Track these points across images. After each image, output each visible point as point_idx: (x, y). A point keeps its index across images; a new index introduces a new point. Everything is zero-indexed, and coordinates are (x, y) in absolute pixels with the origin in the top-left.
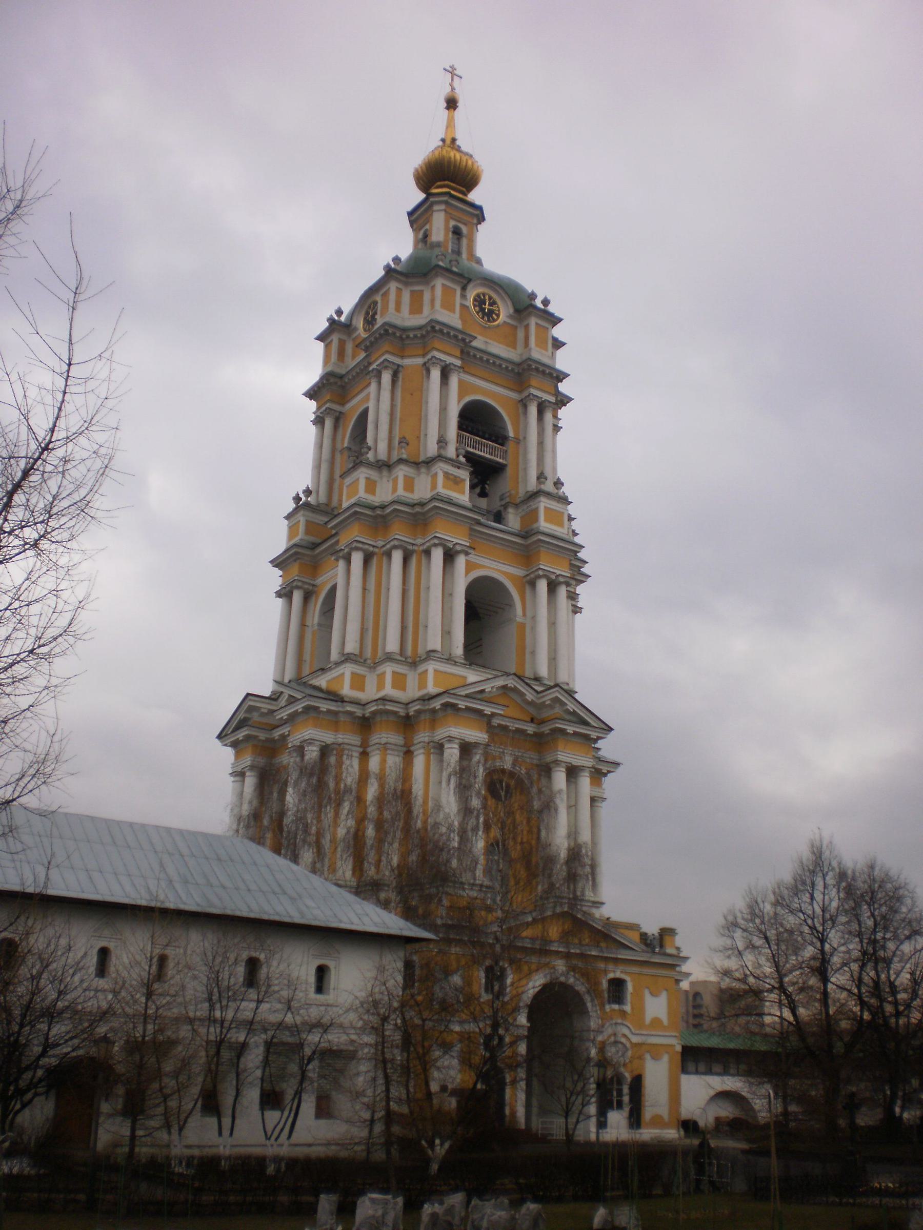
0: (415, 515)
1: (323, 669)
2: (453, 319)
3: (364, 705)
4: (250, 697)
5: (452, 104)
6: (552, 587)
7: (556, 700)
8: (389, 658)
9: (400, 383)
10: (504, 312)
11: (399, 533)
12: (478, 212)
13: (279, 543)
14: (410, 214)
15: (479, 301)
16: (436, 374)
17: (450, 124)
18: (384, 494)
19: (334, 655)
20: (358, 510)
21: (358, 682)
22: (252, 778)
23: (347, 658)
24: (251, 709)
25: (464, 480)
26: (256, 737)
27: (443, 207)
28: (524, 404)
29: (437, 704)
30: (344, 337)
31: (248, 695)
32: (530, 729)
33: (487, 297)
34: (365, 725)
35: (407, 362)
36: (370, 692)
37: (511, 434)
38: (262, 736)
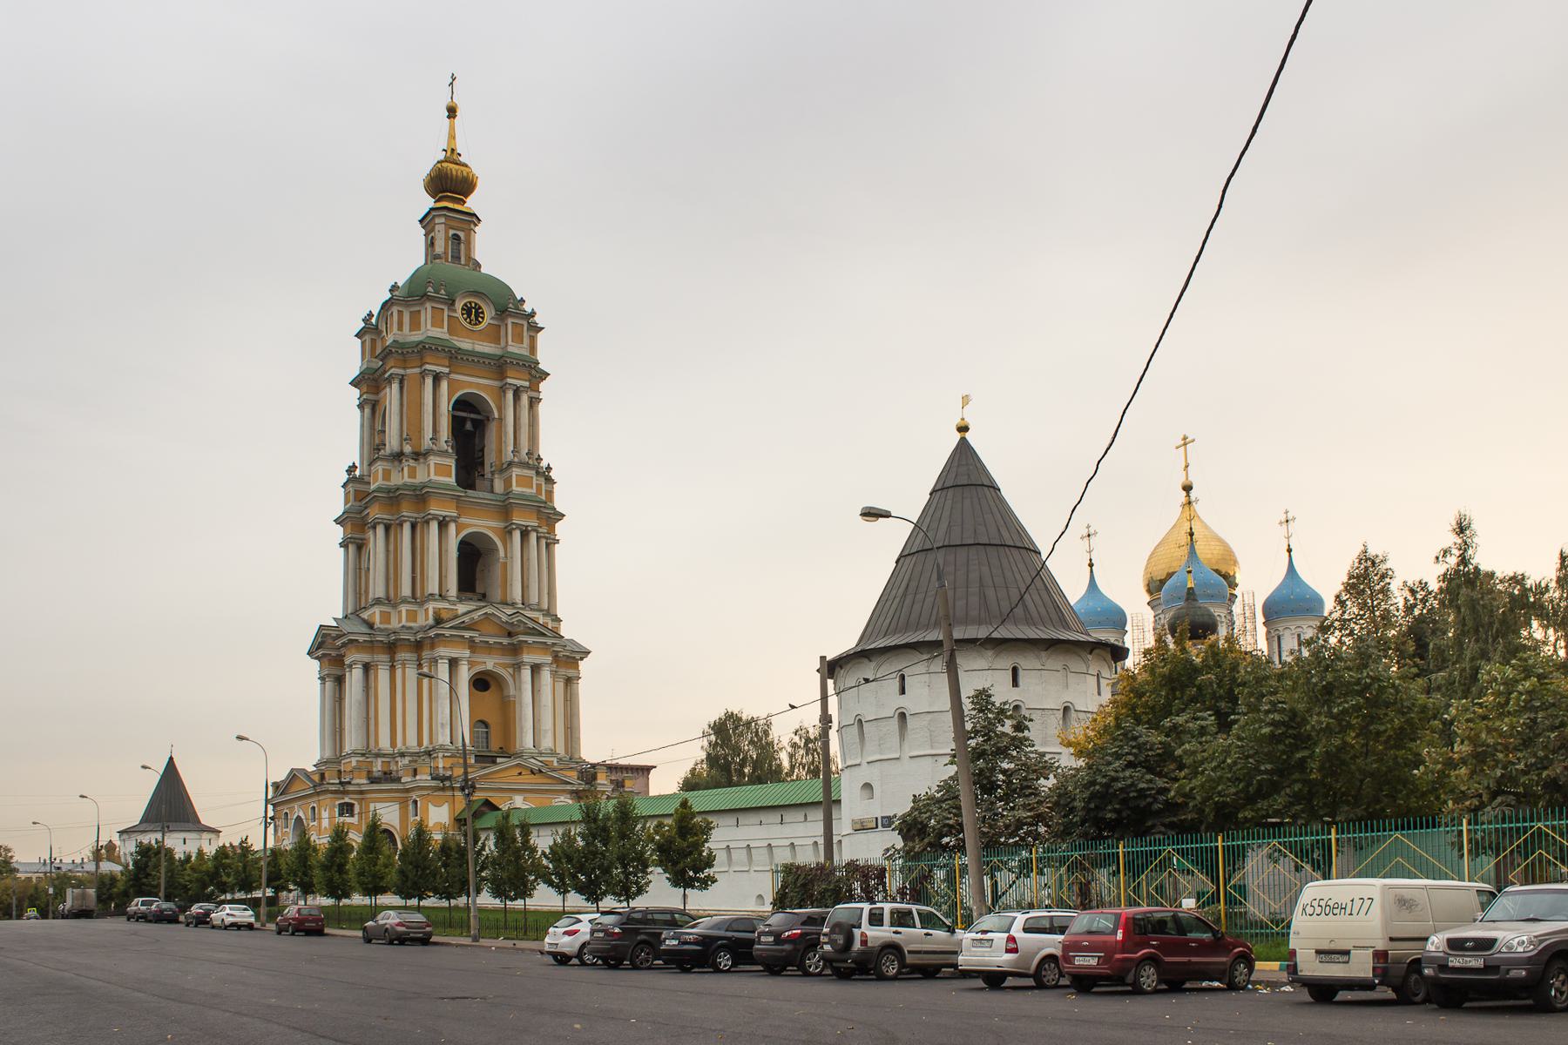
2: (441, 333)
5: (452, 112)
7: (520, 621)
8: (404, 601)
13: (339, 508)
14: (421, 221)
15: (467, 310)
16: (429, 381)
17: (452, 136)
18: (397, 479)
21: (386, 617)
23: (378, 602)
24: (325, 636)
27: (443, 220)
28: (503, 390)
32: (505, 641)
33: (473, 305)
35: (409, 371)
36: (394, 624)
37: (496, 415)
38: (334, 653)
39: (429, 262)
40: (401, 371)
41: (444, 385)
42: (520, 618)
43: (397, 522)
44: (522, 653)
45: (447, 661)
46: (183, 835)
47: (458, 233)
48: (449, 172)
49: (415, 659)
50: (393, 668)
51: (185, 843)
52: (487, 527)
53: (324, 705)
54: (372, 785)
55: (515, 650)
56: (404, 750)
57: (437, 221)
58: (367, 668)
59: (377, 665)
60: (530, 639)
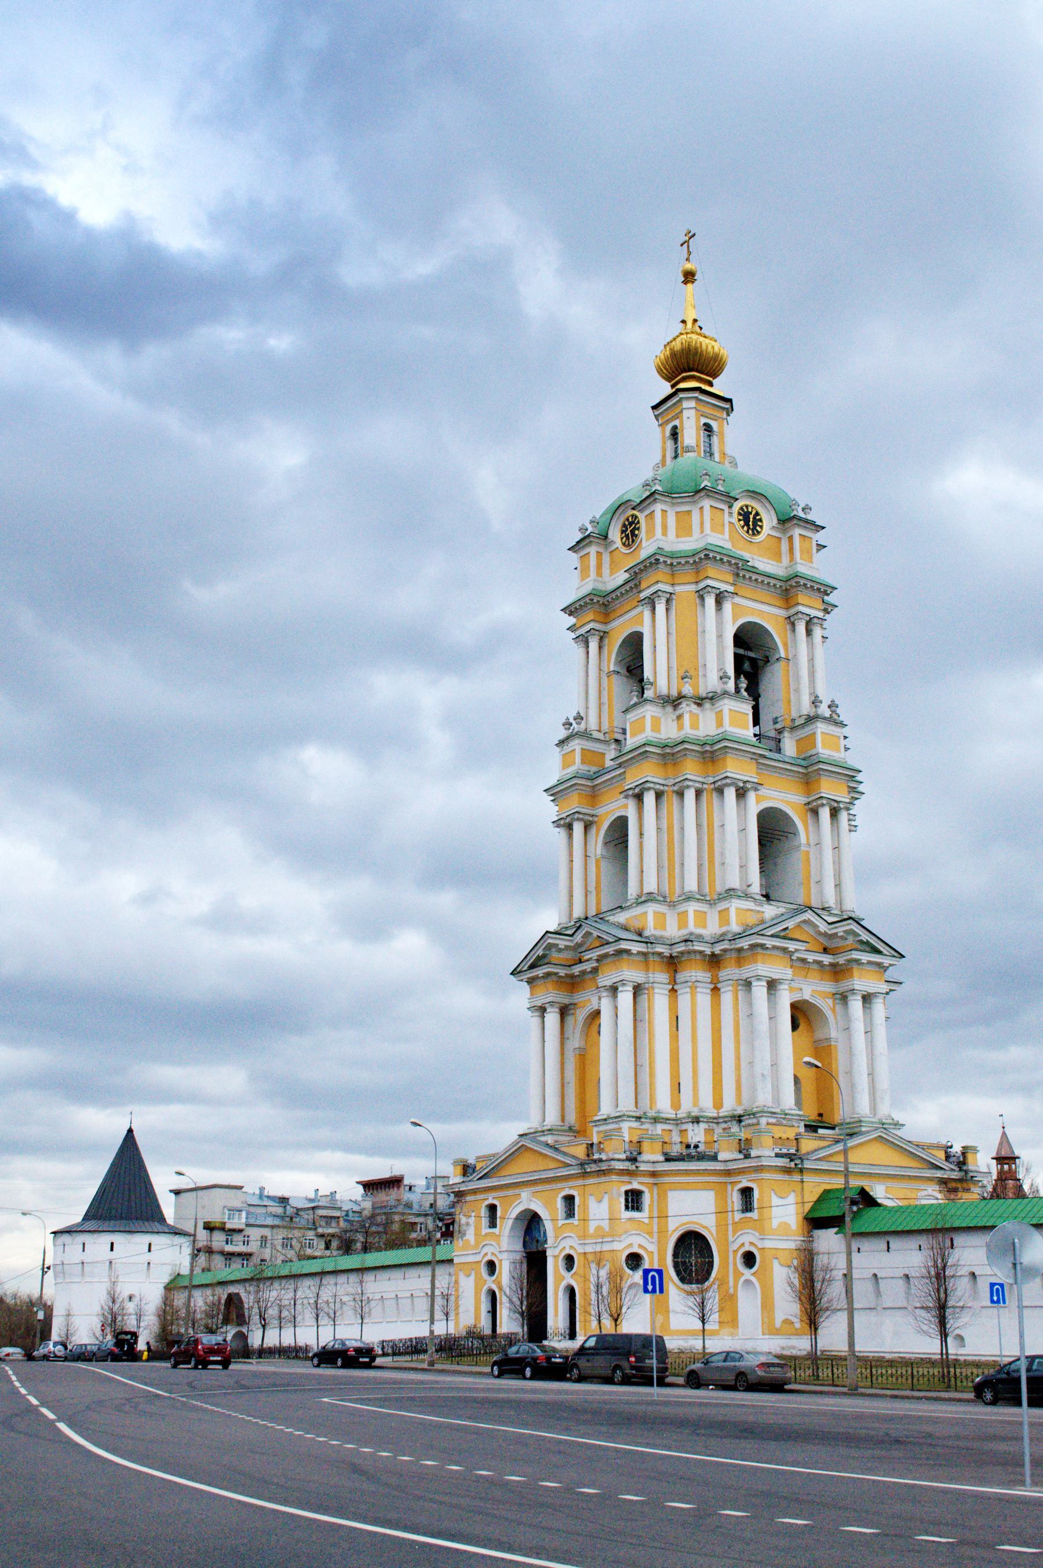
1: (620, 907)
4: (549, 935)
6: (834, 813)
9: (673, 612)
10: (768, 521)
11: (691, 770)
12: (727, 406)
18: (669, 730)
19: (633, 890)
20: (647, 749)
22: (555, 1014)
24: (550, 947)
25: (748, 714)
26: (556, 974)
27: (692, 404)
29: (744, 944)
30: (601, 550)
31: (547, 932)
34: (673, 963)
35: (678, 588)
40: (669, 589)
41: (727, 606)
42: (851, 927)
43: (676, 788)
44: (852, 976)
45: (765, 984)
46: (146, 1239)
48: (698, 345)
49: (709, 980)
50: (716, 990)
51: (112, 1249)
52: (782, 801)
53: (650, 1043)
55: (837, 972)
56: (695, 1112)
58: (638, 990)
59: (653, 988)
60: (865, 957)
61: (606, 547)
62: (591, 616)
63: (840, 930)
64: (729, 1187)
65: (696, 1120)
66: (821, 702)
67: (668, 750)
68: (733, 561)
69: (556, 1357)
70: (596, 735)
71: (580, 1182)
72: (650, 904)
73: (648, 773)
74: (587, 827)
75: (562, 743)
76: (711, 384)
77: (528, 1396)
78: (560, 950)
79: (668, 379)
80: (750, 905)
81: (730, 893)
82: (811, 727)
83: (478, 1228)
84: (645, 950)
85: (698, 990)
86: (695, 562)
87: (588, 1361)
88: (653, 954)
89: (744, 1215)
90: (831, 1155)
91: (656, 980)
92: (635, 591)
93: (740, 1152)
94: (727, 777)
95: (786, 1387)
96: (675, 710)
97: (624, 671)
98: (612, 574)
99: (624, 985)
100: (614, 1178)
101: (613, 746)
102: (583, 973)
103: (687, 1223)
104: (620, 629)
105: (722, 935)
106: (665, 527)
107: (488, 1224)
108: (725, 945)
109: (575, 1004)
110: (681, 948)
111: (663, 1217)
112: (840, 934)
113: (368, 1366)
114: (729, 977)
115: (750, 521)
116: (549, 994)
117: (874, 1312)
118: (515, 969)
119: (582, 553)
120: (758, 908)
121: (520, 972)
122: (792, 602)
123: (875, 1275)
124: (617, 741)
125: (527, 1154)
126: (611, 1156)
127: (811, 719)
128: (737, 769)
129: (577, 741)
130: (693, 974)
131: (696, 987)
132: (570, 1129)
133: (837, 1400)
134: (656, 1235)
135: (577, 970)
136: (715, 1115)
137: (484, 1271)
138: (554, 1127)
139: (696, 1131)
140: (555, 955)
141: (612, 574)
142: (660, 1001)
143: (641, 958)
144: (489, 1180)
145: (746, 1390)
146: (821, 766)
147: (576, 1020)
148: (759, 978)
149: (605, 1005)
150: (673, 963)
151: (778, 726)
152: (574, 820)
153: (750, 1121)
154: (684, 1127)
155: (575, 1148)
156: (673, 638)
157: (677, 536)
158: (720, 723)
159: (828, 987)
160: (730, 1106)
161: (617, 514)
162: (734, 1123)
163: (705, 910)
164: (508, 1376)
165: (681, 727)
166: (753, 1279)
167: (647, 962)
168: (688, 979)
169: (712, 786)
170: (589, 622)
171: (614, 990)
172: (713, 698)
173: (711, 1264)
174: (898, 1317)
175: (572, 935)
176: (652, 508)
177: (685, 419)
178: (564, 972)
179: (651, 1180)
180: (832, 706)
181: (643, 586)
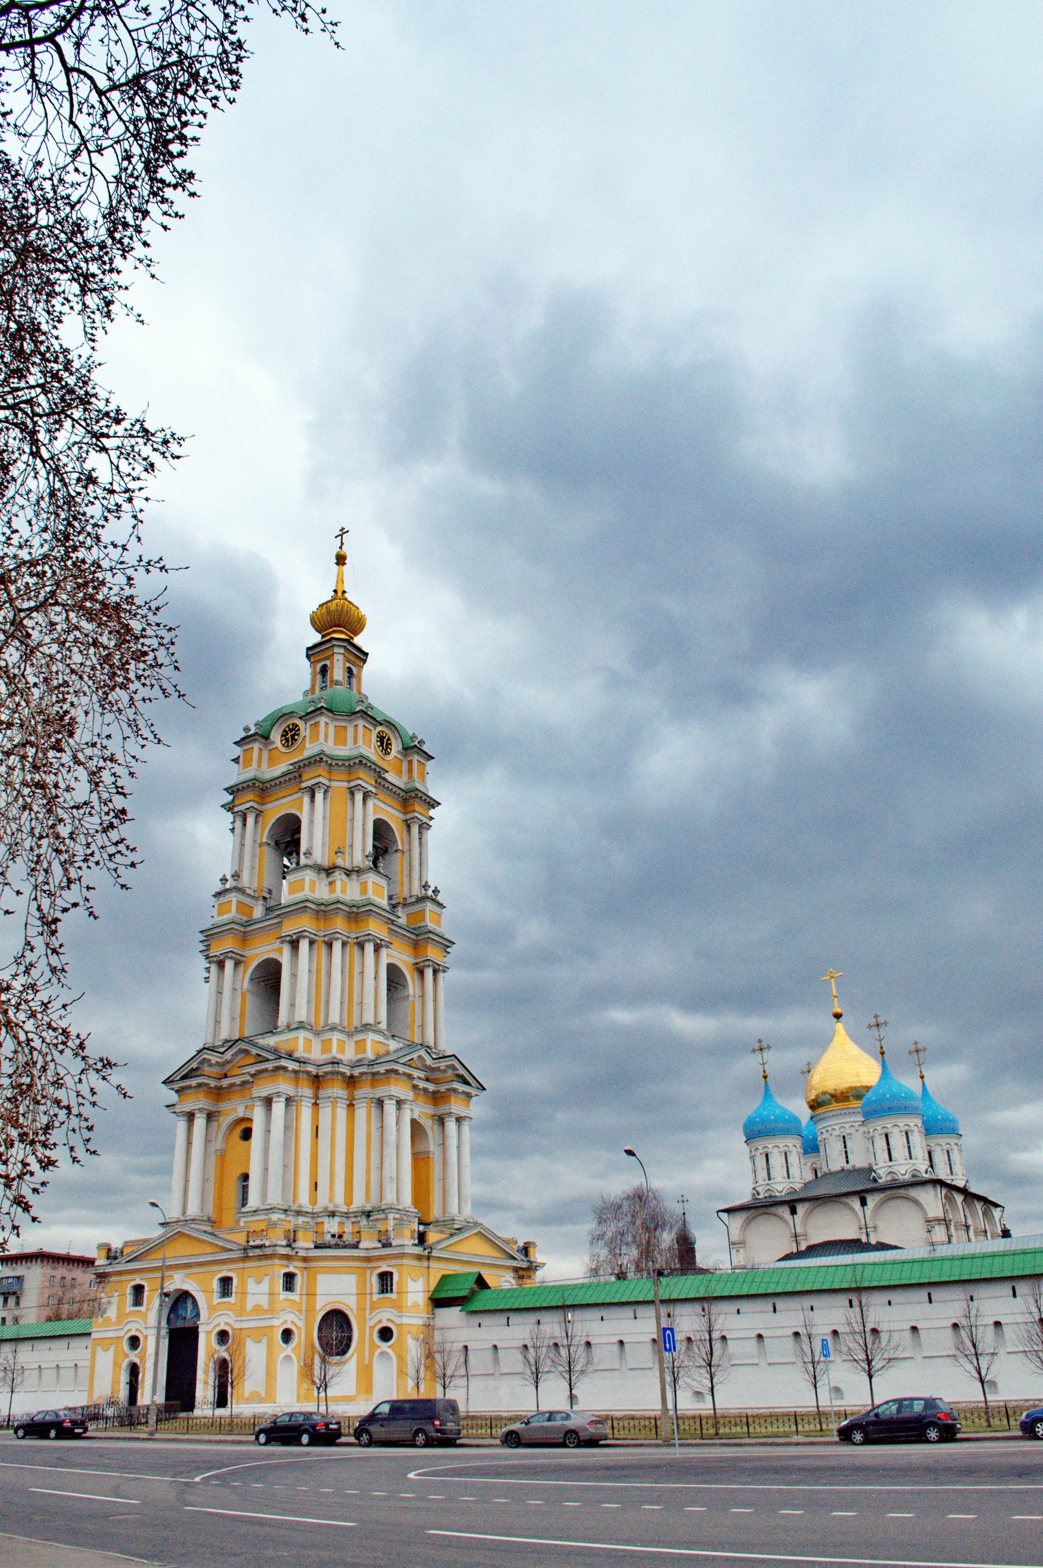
0: (349, 913)
1: (272, 1032)
3: (318, 1066)
4: (206, 1051)
10: (396, 747)
11: (339, 924)
17: (340, 580)
19: (283, 1019)
27: (342, 651)
30: (261, 747)
34: (317, 1081)
35: (334, 784)
39: (317, 689)
40: (327, 782)
43: (326, 939)
45: (394, 1102)
47: (352, 667)
49: (345, 1097)
50: (351, 1105)
54: (385, 1249)
56: (331, 1208)
57: (336, 650)
60: (462, 1087)
61: (266, 745)
62: (251, 797)
63: (443, 1064)
64: (368, 1272)
65: (333, 1214)
66: (429, 887)
67: (323, 908)
68: (378, 770)
69: (332, 1424)
70: (248, 891)
71: (241, 1265)
72: (302, 1031)
73: (305, 923)
74: (237, 964)
75: (218, 895)
76: (352, 639)
77: (540, 1461)
78: (211, 1065)
79: (318, 631)
80: (379, 1038)
81: (366, 1027)
82: (422, 905)
83: (120, 1308)
84: (297, 1068)
85: (339, 1105)
86: (349, 765)
87: (382, 1426)
88: (303, 1072)
89: (382, 1296)
90: (447, 1246)
91: (304, 1094)
92: (298, 780)
93: (380, 1241)
94: (369, 934)
95: (600, 1442)
96: (328, 877)
97: (273, 844)
98: (269, 767)
99: (279, 1096)
100: (277, 1261)
101: (261, 902)
102: (232, 1085)
103: (333, 1302)
104: (277, 808)
105: (358, 1061)
106: (326, 736)
107: (132, 1303)
108: (364, 1069)
109: (219, 1112)
110: (328, 1068)
111: (311, 1294)
112: (442, 1068)
113: (78, 1437)
114: (365, 1095)
115: (384, 743)
116: (197, 1102)
117: (491, 1378)
118: (168, 1078)
119: (245, 748)
120: (386, 1042)
121: (172, 1081)
122: (410, 809)
123: (495, 1347)
124: (265, 898)
125: (185, 1240)
126: (275, 1242)
127: (421, 900)
128: (376, 928)
129: (234, 894)
130: (335, 1091)
131: (337, 1102)
132: (209, 1220)
133: (655, 1450)
134: (304, 1313)
135: (225, 1082)
136: (346, 1211)
137: (125, 1346)
138: (198, 1218)
139: (331, 1224)
140: (207, 1069)
141: (269, 767)
142: (306, 1112)
143: (292, 1075)
144: (139, 1263)
145: (578, 1446)
146: (431, 936)
147: (219, 1127)
148: (391, 1097)
149: (258, 1114)
150: (317, 1081)
151: (393, 902)
152: (227, 957)
153: (379, 1216)
154: (320, 1220)
155: (235, 1235)
156: (328, 820)
157: (335, 744)
158: (364, 891)
159: (429, 1110)
160: (359, 1202)
161: (279, 722)
162: (364, 1217)
163: (345, 1039)
164: (273, 1443)
165: (332, 891)
166: (389, 1351)
167: (297, 1079)
168: (330, 1095)
169: (355, 940)
170: (248, 801)
171: (268, 1102)
172: (359, 871)
173: (350, 1339)
174: (517, 1381)
175: (222, 1053)
176: (317, 720)
177: (335, 661)
178: (215, 1083)
179: (302, 1264)
180: (436, 891)
181: (304, 778)
